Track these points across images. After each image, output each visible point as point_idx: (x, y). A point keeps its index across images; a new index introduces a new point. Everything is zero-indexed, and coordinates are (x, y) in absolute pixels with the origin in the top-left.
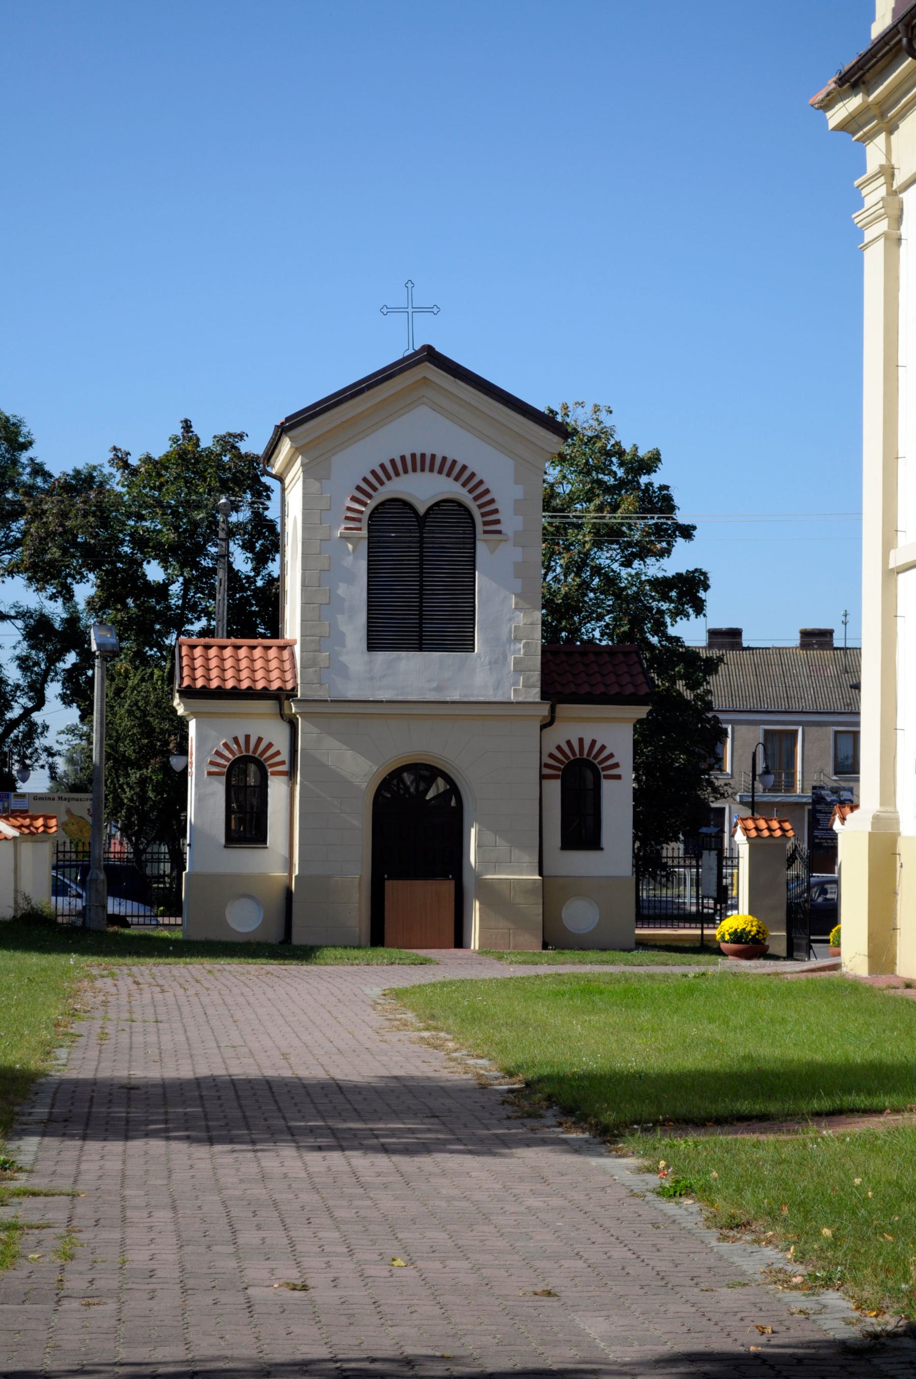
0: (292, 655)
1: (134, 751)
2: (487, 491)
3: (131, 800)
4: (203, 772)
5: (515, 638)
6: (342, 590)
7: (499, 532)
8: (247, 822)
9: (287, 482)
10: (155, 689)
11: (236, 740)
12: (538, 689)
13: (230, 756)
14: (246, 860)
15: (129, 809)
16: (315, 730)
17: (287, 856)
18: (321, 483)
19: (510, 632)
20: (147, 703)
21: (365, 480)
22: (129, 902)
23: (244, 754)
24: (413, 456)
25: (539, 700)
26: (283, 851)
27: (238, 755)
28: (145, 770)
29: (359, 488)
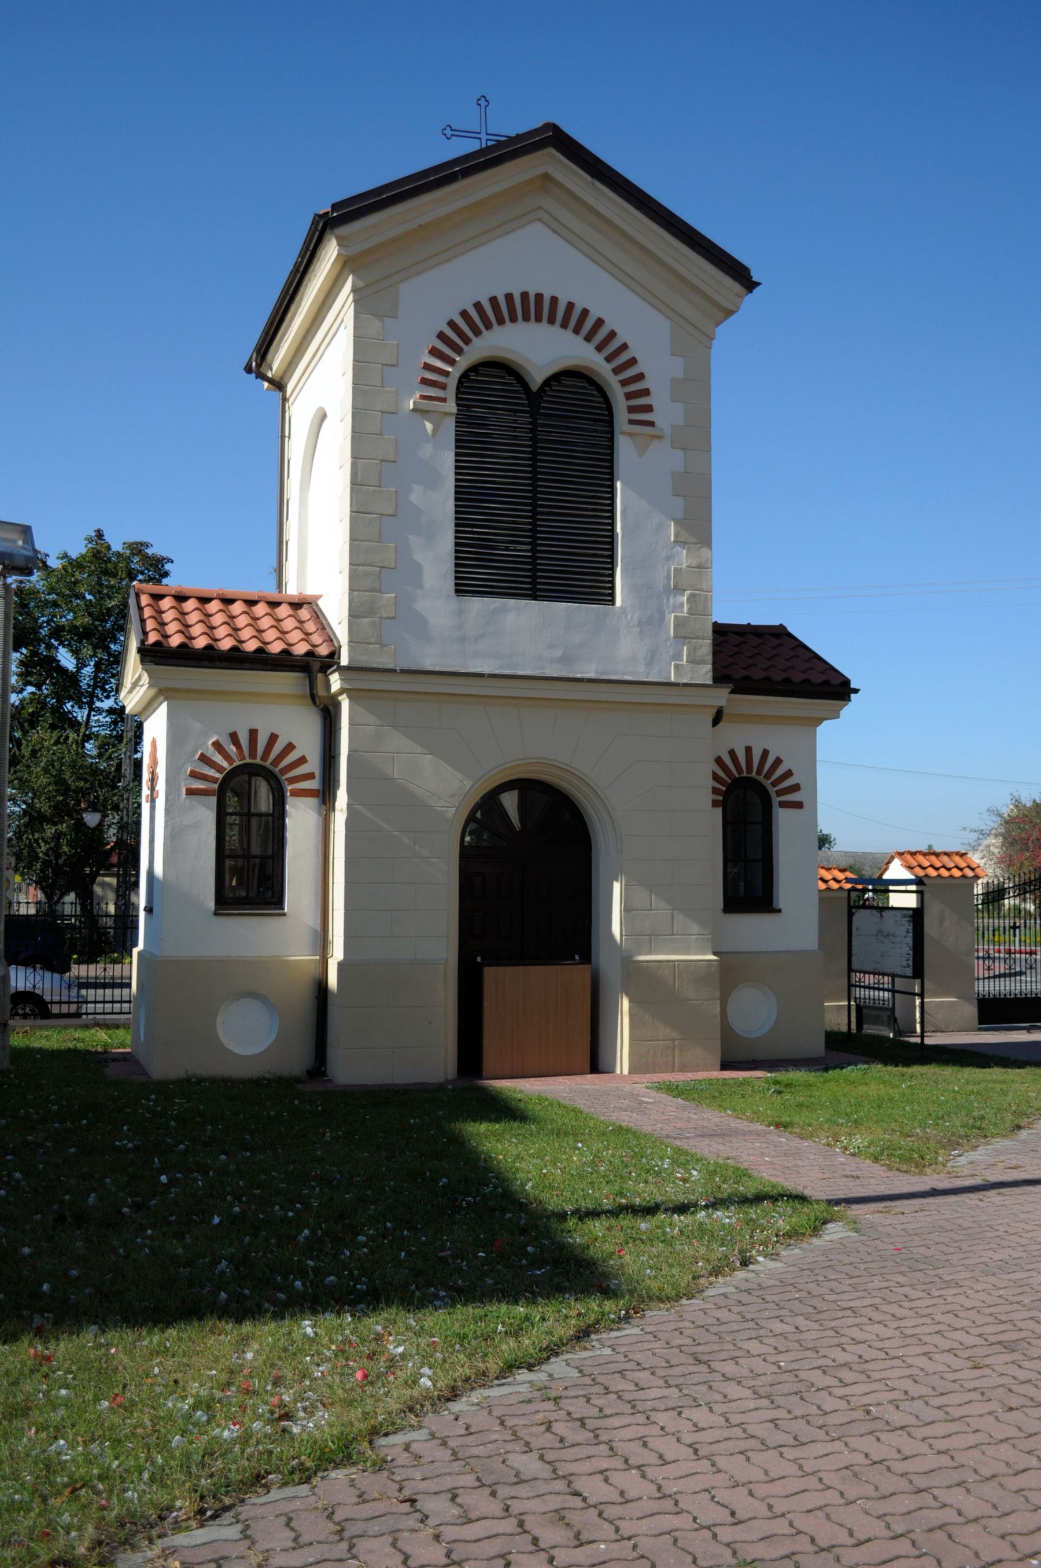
0: (318, 616)
1: (50, 807)
2: (633, 361)
3: (46, 854)
4: (179, 788)
5: (676, 587)
6: (417, 496)
7: (651, 424)
8: (250, 877)
9: (289, 388)
10: (69, 752)
11: (234, 737)
12: (709, 667)
13: (225, 764)
14: (251, 936)
15: (46, 864)
16: (373, 720)
17: (319, 929)
18: (383, 322)
19: (668, 577)
20: (62, 764)
21: (452, 324)
22: (48, 975)
23: (248, 760)
24: (525, 295)
25: (710, 682)
29: (441, 336)
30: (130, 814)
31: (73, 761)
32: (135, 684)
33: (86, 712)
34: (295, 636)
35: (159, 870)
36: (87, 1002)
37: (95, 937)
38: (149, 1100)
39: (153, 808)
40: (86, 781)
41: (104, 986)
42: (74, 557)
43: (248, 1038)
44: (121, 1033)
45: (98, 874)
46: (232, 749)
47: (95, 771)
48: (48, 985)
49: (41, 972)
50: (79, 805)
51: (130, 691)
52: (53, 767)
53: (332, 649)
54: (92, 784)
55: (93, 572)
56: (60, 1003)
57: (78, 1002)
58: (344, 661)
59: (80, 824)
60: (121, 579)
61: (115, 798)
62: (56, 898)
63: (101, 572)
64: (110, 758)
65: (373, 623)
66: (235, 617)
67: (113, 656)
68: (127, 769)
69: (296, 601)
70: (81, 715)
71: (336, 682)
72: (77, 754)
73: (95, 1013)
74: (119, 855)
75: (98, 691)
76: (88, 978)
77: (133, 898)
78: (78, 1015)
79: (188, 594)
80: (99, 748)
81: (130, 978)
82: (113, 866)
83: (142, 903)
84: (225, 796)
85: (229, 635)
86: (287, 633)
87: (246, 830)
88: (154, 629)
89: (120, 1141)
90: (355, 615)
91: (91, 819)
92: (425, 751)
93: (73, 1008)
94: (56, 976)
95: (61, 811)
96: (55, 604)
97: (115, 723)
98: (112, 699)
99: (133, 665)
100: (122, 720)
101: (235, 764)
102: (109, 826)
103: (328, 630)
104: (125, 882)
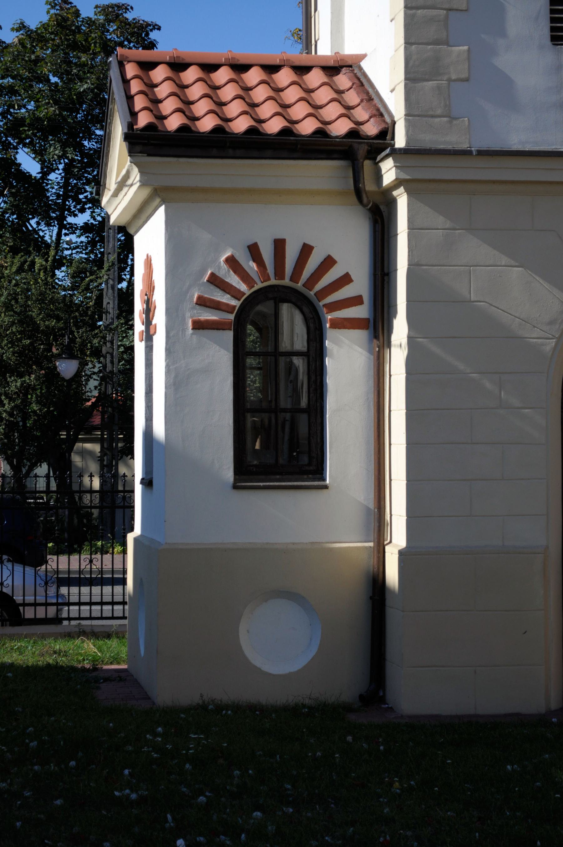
0: (362, 83)
1: (14, 353)
3: (11, 414)
8: (279, 437)
10: (36, 282)
13: (243, 287)
14: (283, 517)
16: (440, 221)
17: (372, 505)
22: (18, 568)
23: (273, 281)
26: (359, 492)
27: (259, 285)
28: (27, 377)
30: (116, 361)
31: (41, 294)
32: (122, 184)
33: (56, 230)
34: (332, 111)
35: (159, 429)
36: (69, 604)
37: (76, 521)
38: (156, 735)
39: (149, 349)
40: (58, 319)
41: (91, 582)
42: (33, 27)
43: (281, 652)
44: (114, 643)
45: (77, 440)
46: (252, 267)
47: (68, 305)
48: (18, 582)
49: (10, 565)
50: (50, 350)
51: (116, 194)
52: (17, 302)
53: (382, 126)
54: (65, 323)
55: (58, 46)
56: (35, 604)
57: (57, 604)
58: (400, 141)
59: (53, 375)
60: (95, 54)
61: (95, 341)
62: (24, 471)
63: (68, 46)
64: (87, 289)
65: (439, 88)
66: (251, 89)
67: (88, 155)
68: (110, 303)
69: (331, 63)
70: (49, 234)
71: (389, 171)
72: (46, 284)
73: (80, 618)
74: (103, 413)
75: (70, 203)
76: (69, 572)
77: (122, 470)
78: (57, 620)
79: (188, 60)
80: (73, 277)
81: (125, 572)
82: (96, 428)
83: (139, 474)
84: (245, 329)
85: (244, 113)
86: (321, 107)
87: (270, 376)
88: (145, 109)
89: (121, 790)
90: (413, 77)
91: (67, 368)
92: (513, 263)
93: (52, 611)
94: (29, 570)
95: (29, 359)
96: (12, 91)
97: (92, 243)
98: (88, 212)
99: (118, 159)
100: (102, 240)
101: (256, 288)
102: (89, 377)
103: (376, 101)
104: (110, 448)
